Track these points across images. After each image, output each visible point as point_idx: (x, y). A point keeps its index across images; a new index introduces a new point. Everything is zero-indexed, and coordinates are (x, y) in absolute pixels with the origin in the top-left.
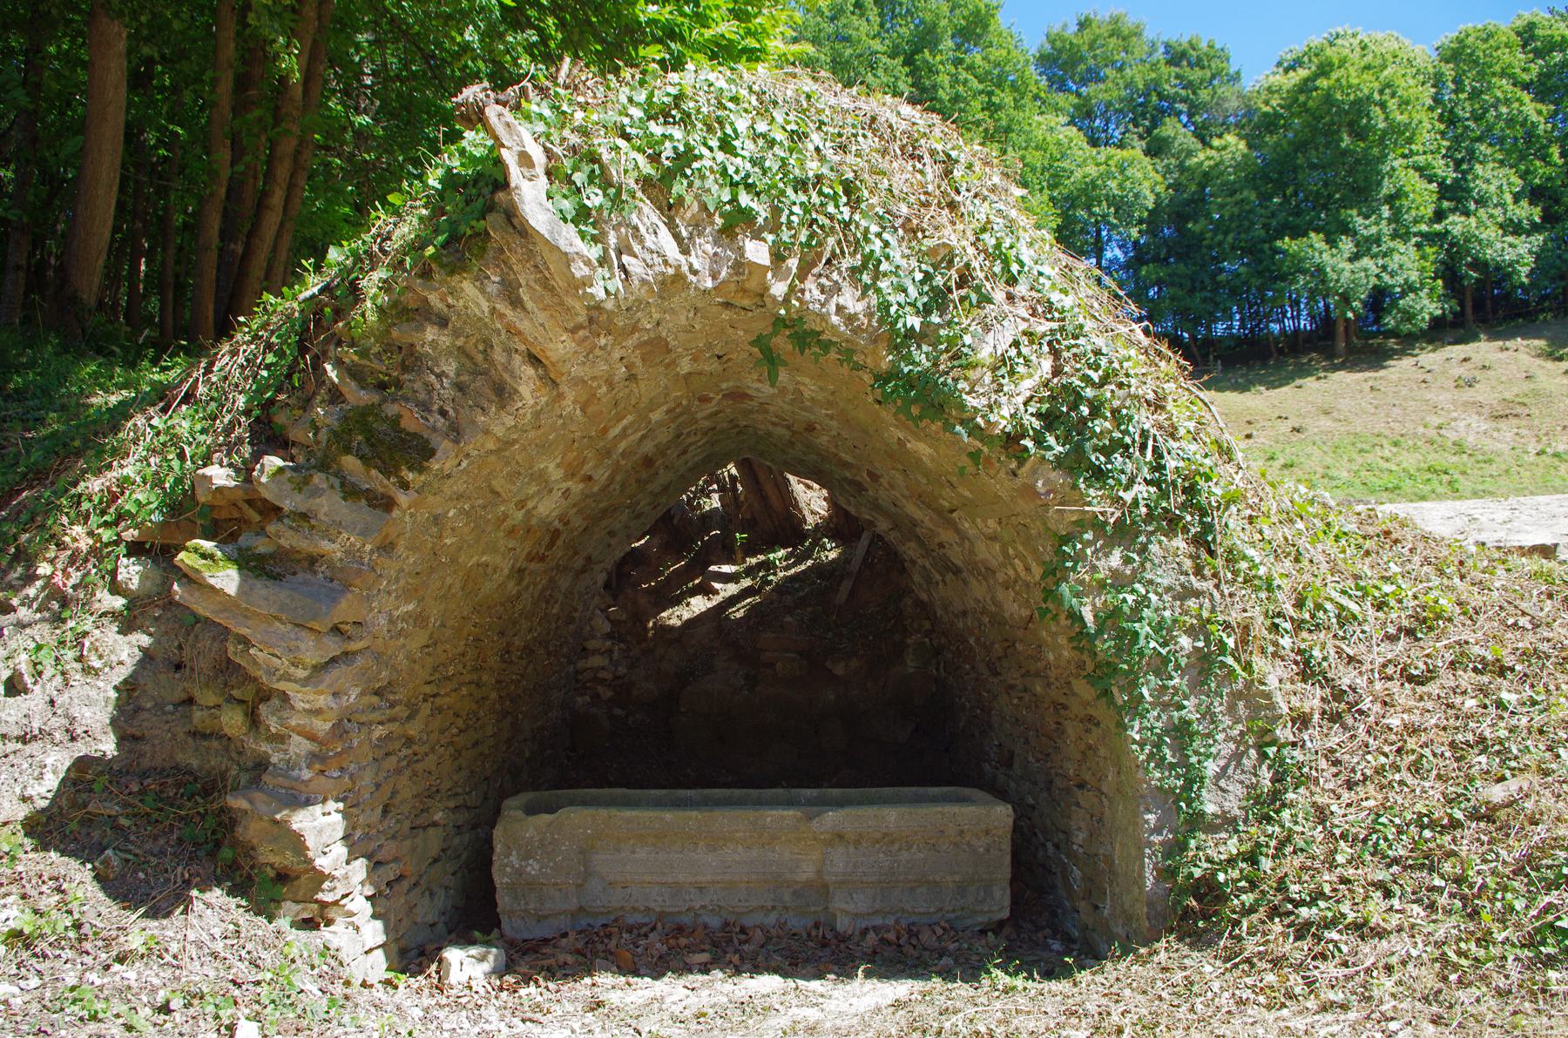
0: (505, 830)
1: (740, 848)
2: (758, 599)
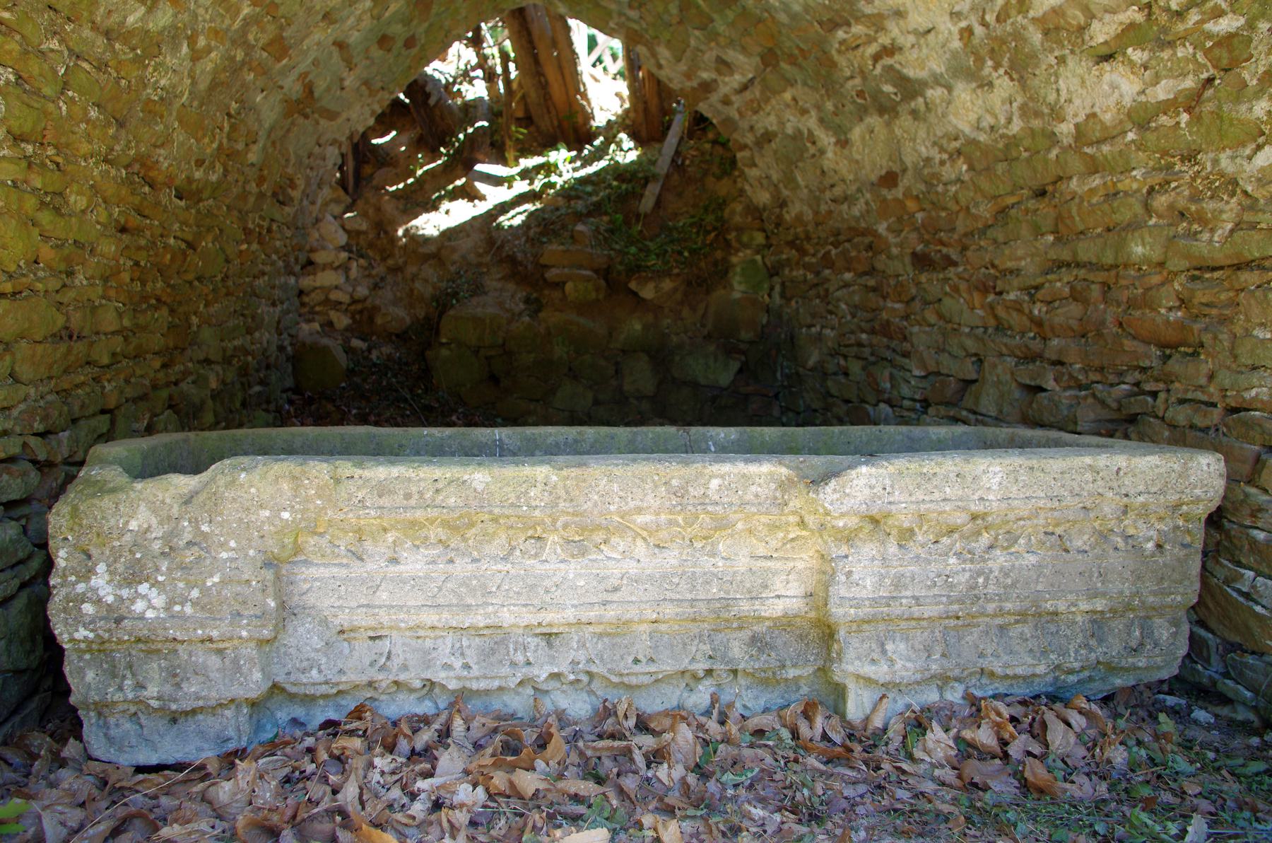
0: (75, 513)
1: (640, 549)
2: (538, 205)
